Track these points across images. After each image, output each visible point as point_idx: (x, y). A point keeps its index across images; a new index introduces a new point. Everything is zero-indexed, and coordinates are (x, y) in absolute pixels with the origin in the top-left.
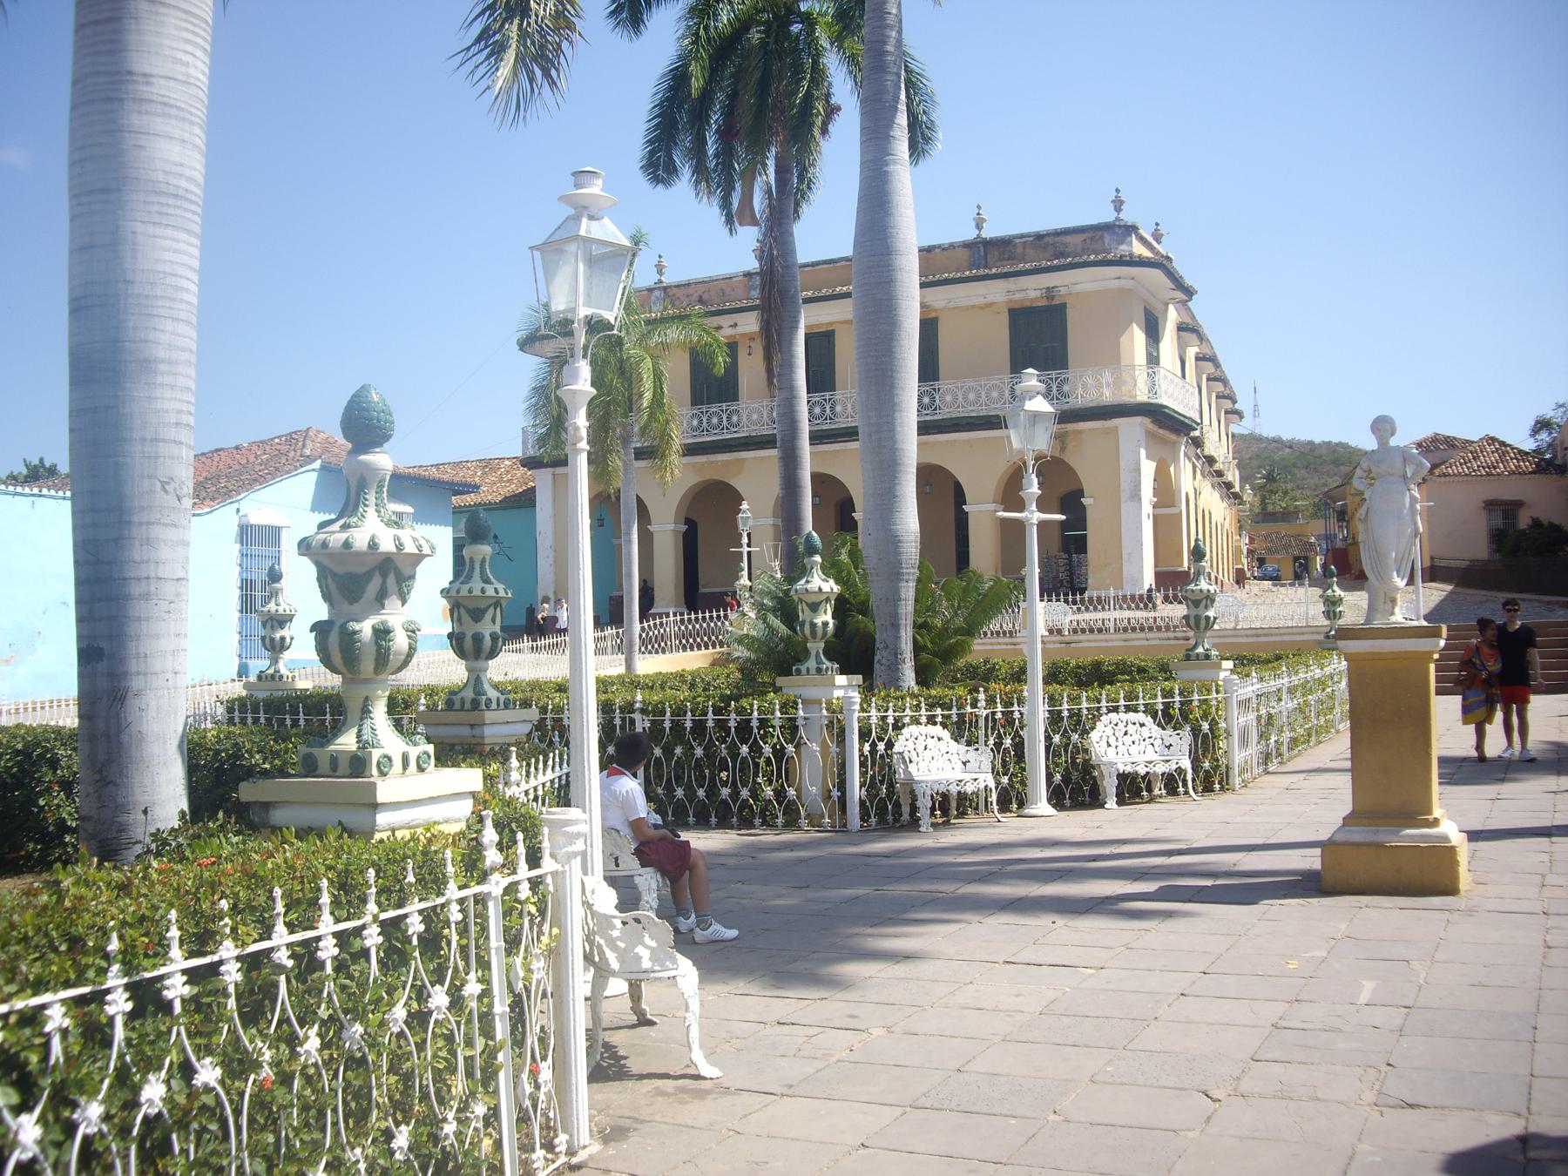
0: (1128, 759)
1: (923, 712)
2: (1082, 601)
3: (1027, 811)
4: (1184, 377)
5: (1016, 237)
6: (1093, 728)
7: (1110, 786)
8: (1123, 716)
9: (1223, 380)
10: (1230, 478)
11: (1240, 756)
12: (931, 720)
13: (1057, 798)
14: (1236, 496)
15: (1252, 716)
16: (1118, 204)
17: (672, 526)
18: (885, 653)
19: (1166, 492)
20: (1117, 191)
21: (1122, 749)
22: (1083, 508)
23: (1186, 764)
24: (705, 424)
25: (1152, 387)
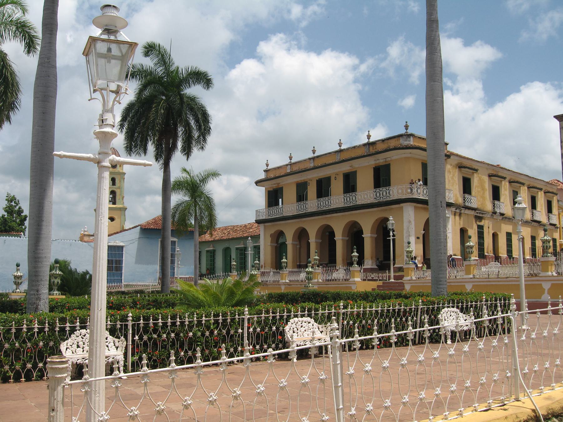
5: (376, 141)
8: (300, 319)
16: (407, 127)
20: (406, 122)
21: (299, 333)
24: (381, 195)
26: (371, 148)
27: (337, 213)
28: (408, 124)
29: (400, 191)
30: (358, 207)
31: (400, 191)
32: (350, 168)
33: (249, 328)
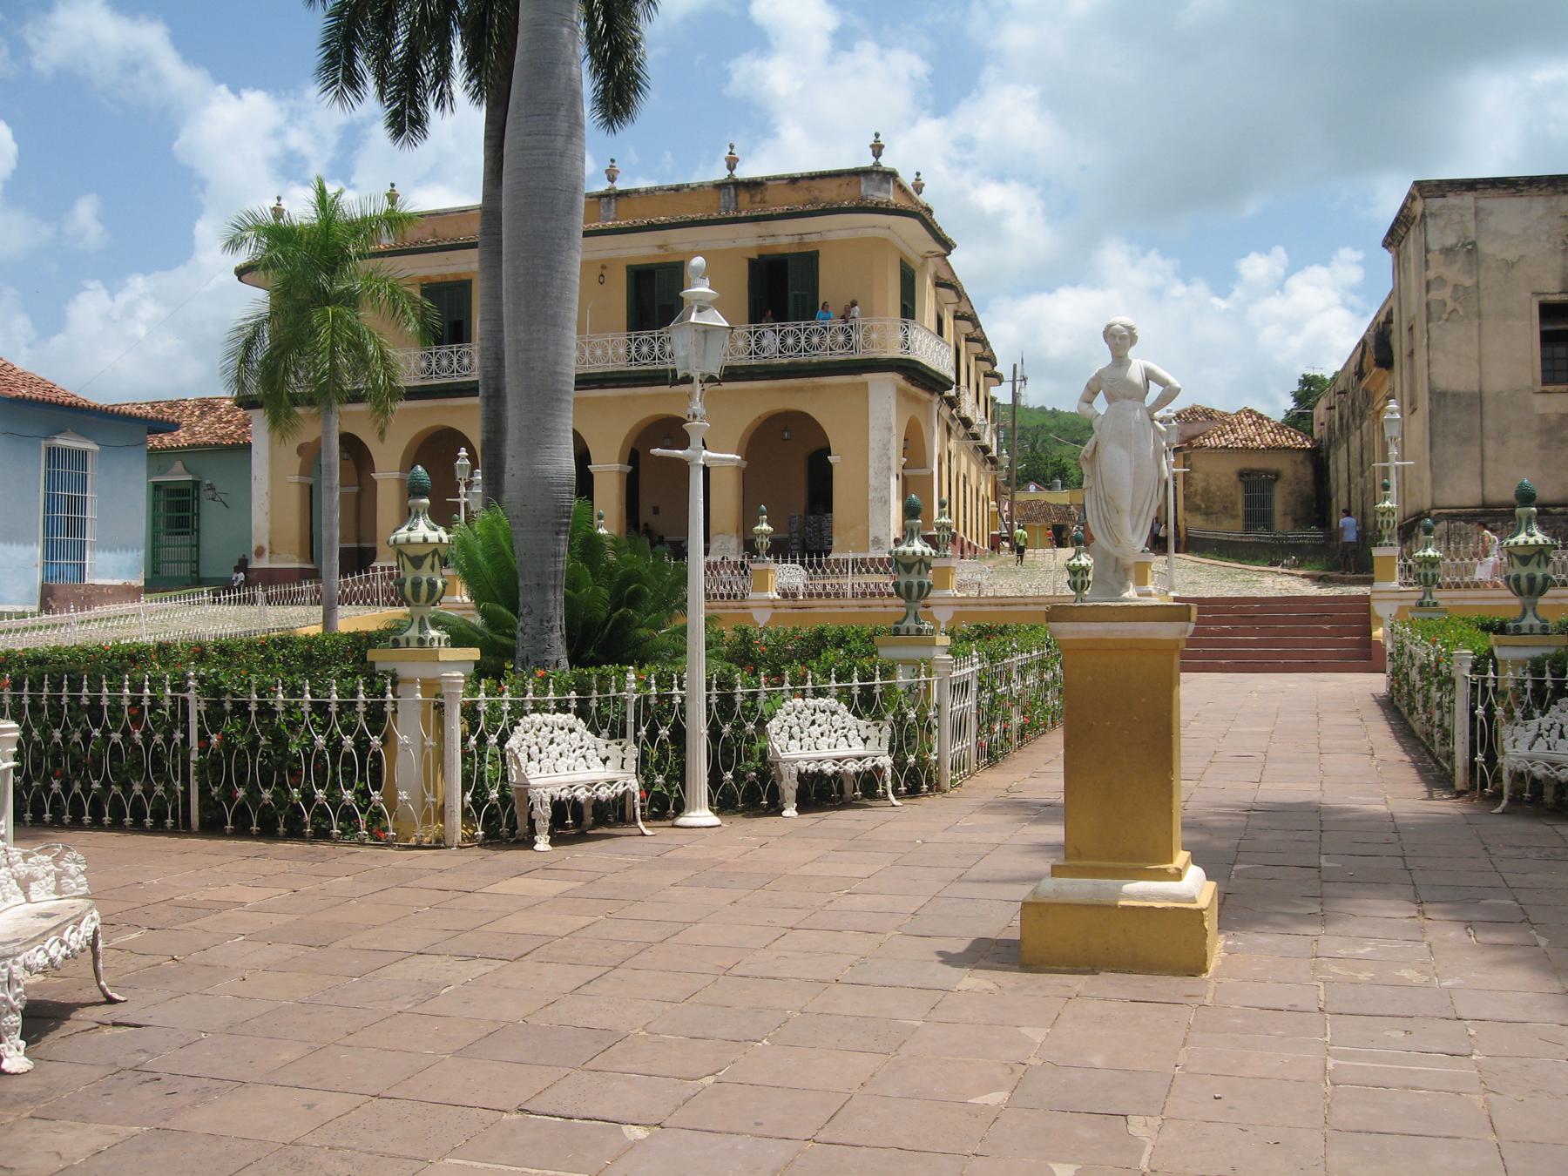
0: (814, 754)
1: (551, 695)
2: (819, 564)
3: (681, 821)
4: (940, 332)
5: (768, 179)
6: (772, 716)
7: (789, 788)
8: (810, 702)
9: (983, 341)
10: (986, 441)
11: (946, 749)
12: (562, 708)
13: (723, 803)
14: (993, 461)
15: (970, 702)
16: (877, 149)
17: (397, 475)
18: (528, 620)
19: (914, 448)
20: (877, 135)
21: (807, 741)
22: (830, 467)
23: (886, 761)
24: (455, 365)
25: (905, 344)
26: (744, 198)
27: (601, 387)
28: (882, 140)
29: (599, 352)
30: (612, 380)
31: (599, 352)
32: (656, 251)
33: (637, 729)
